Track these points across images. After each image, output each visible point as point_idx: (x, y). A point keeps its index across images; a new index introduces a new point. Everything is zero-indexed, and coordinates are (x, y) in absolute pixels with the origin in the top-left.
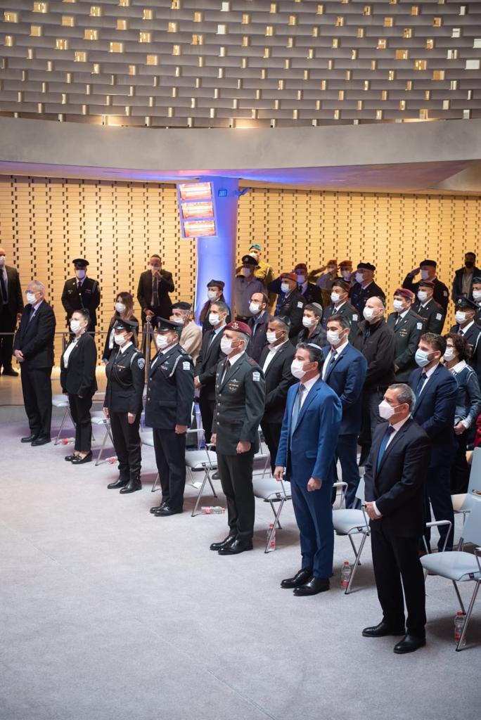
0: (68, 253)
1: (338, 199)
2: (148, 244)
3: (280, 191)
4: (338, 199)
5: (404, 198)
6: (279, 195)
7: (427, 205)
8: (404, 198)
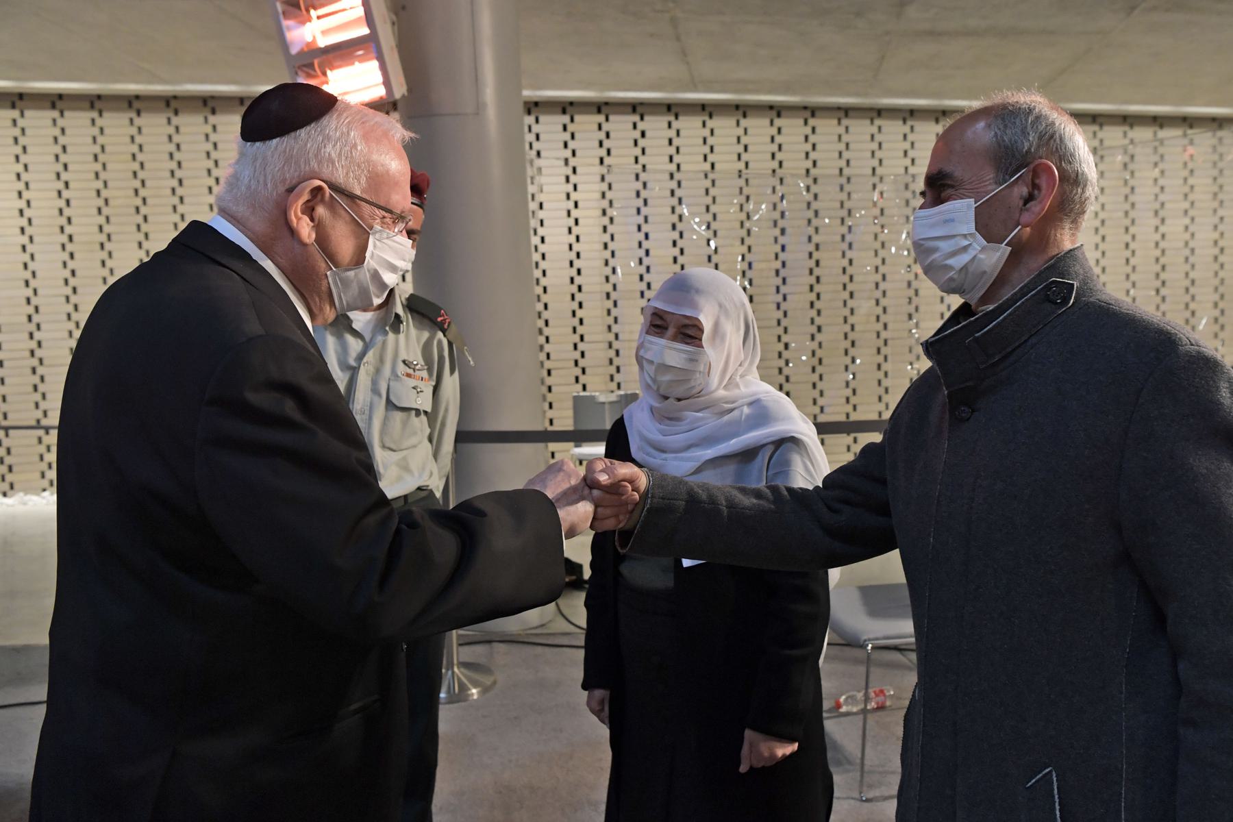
3: (842, 114)
5: (1101, 125)
8: (1101, 125)
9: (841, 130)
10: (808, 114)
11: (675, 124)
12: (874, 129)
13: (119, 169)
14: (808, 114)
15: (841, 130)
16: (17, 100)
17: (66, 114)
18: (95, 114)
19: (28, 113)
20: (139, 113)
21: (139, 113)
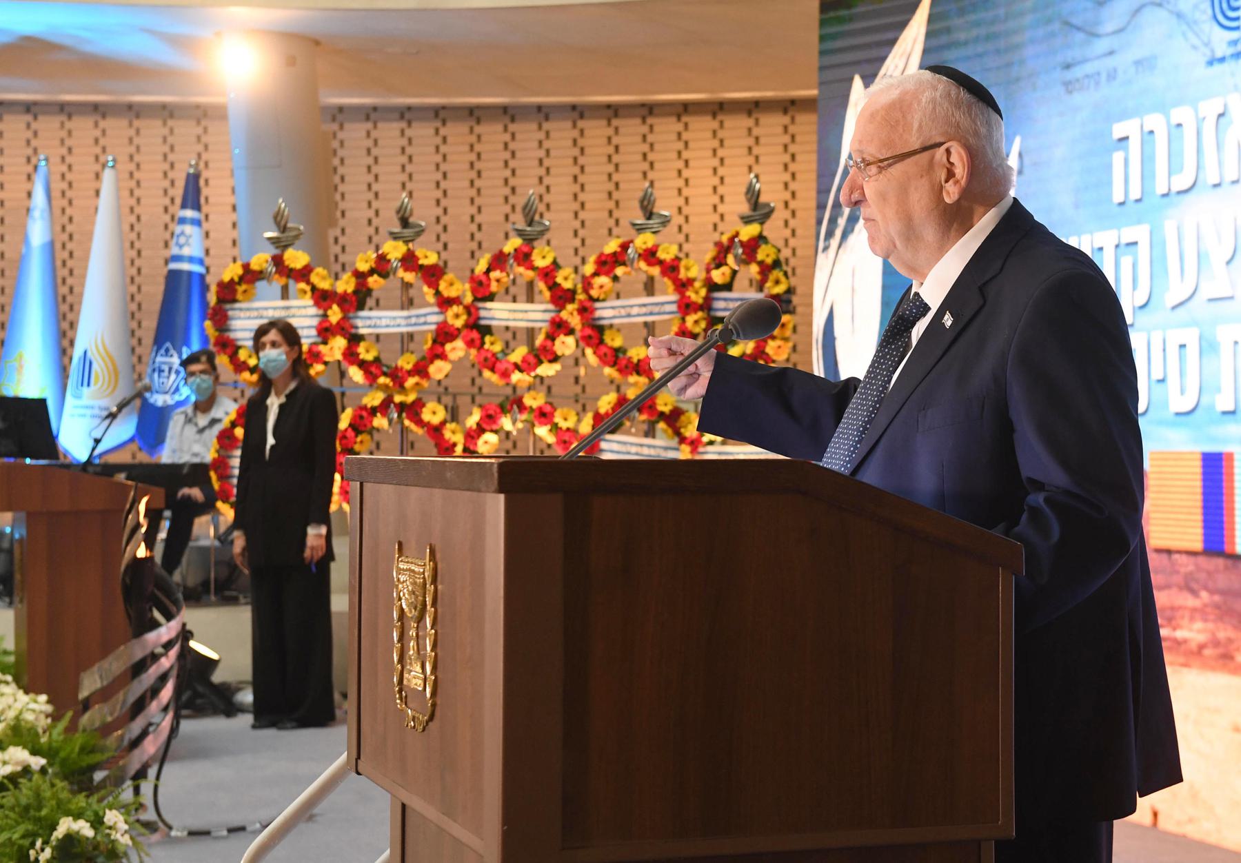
1: (757, 123)
4: (757, 123)
6: (609, 124)
7: (576, 133)
9: (610, 131)
10: (576, 115)
11: (443, 131)
13: (1190, 503)
14: (576, 115)
15: (645, 129)
17: (380, 125)
18: (403, 124)
20: (409, 123)
21: (444, 123)
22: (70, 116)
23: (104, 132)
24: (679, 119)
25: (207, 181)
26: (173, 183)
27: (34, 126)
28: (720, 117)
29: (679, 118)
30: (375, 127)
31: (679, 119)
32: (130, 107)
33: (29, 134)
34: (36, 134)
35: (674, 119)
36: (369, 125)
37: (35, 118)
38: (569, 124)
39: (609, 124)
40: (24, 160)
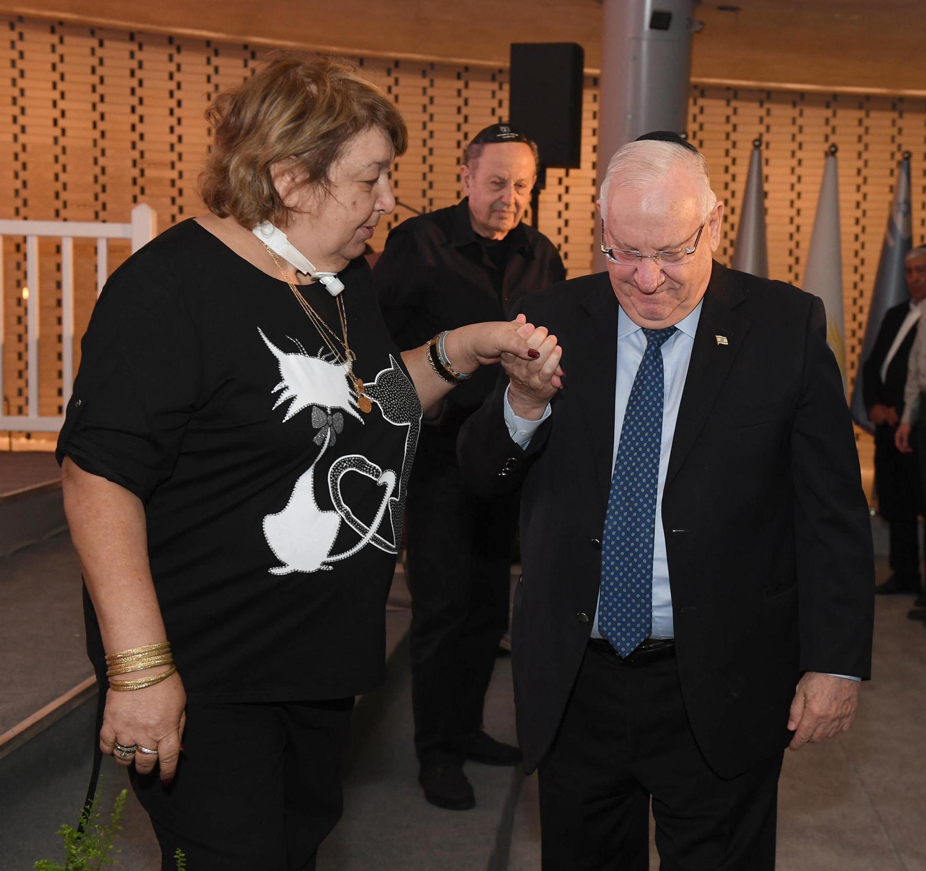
0: (430, 194)
2: (566, 198)
6: (728, 105)
7: (210, 70)
10: (247, 54)
12: (729, 111)
14: (247, 54)
16: (15, 22)
19: (840, 113)
21: (179, 50)
22: (179, 50)
23: (216, 70)
24: (761, 105)
25: (566, 255)
26: (861, 294)
27: (899, 123)
28: (766, 106)
29: (389, 73)
30: (867, 115)
31: (761, 105)
32: (171, 39)
33: (894, 131)
34: (900, 131)
35: (757, 105)
36: (460, 84)
37: (901, 116)
38: (240, 62)
39: (728, 105)
40: (789, 171)
